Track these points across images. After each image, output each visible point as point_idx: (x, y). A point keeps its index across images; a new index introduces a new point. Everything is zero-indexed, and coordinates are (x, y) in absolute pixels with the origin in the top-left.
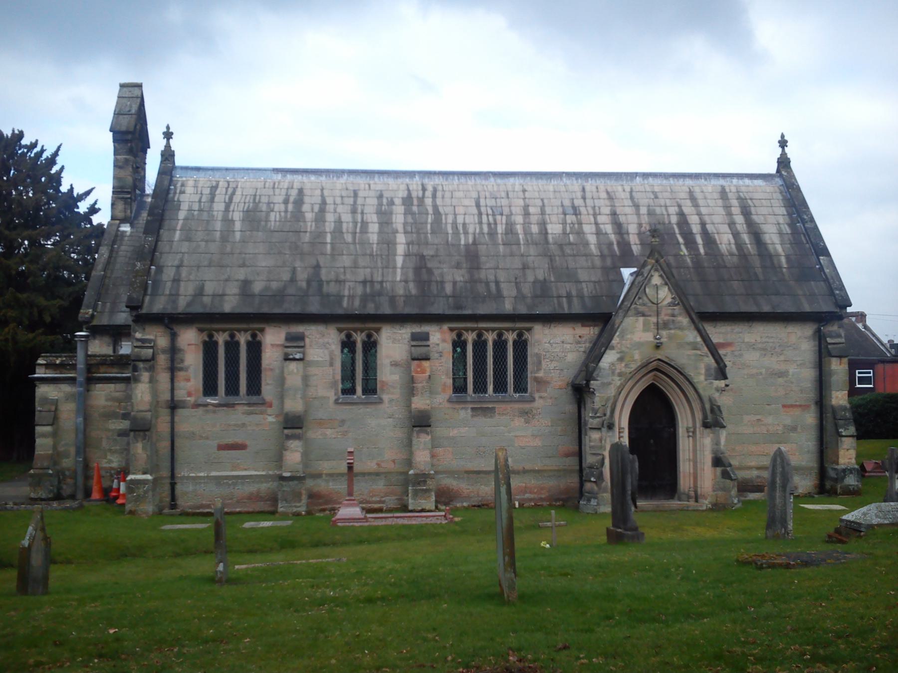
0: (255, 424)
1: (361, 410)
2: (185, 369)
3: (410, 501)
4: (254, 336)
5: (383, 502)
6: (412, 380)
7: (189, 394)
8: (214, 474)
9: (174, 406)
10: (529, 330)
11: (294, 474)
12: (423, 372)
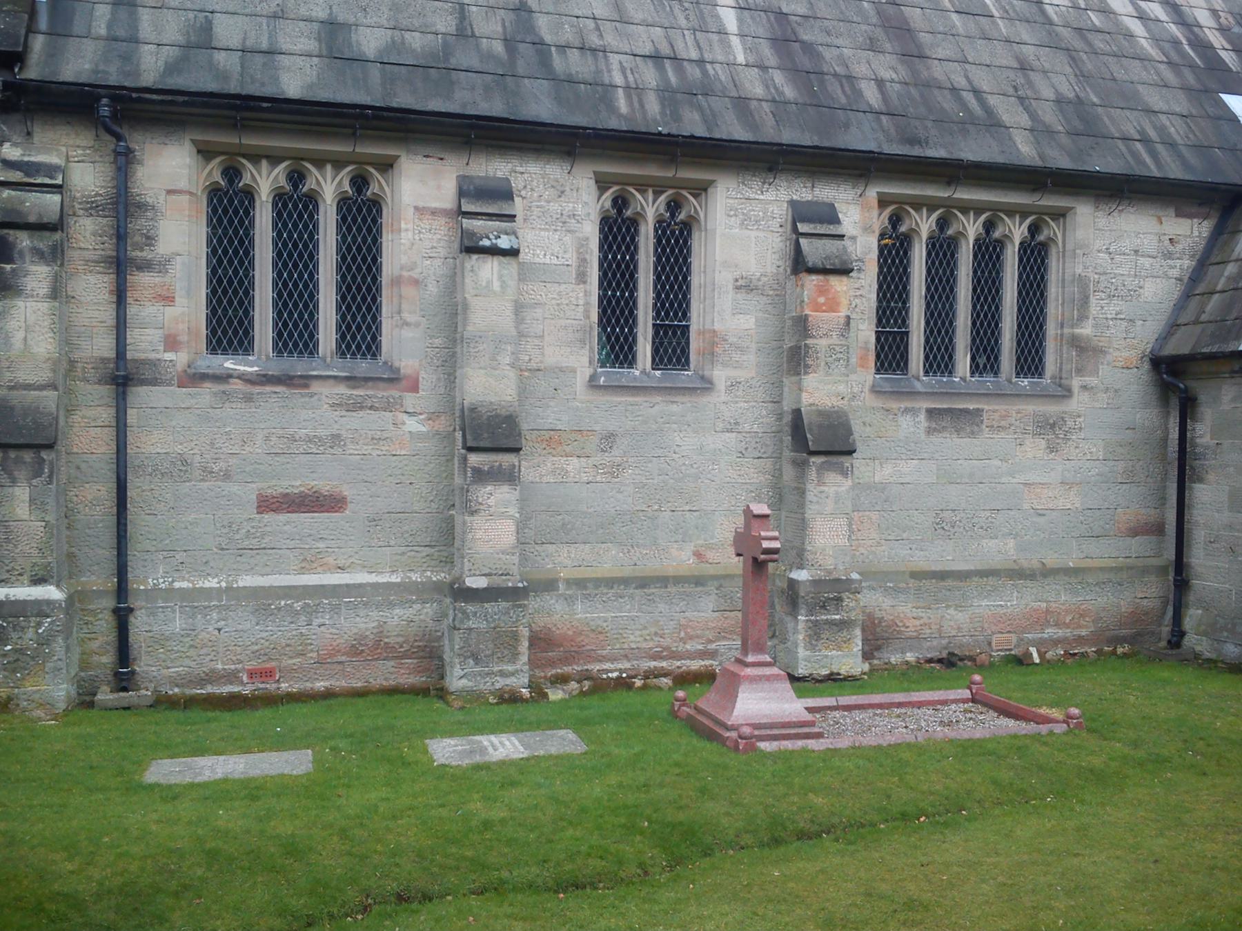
0: (376, 441)
1: (655, 408)
2: (161, 266)
3: (802, 652)
4: (360, 182)
5: (713, 654)
6: (802, 325)
7: (171, 343)
8: (247, 581)
9: (123, 377)
10: (1060, 215)
11: (498, 581)
12: (832, 306)
